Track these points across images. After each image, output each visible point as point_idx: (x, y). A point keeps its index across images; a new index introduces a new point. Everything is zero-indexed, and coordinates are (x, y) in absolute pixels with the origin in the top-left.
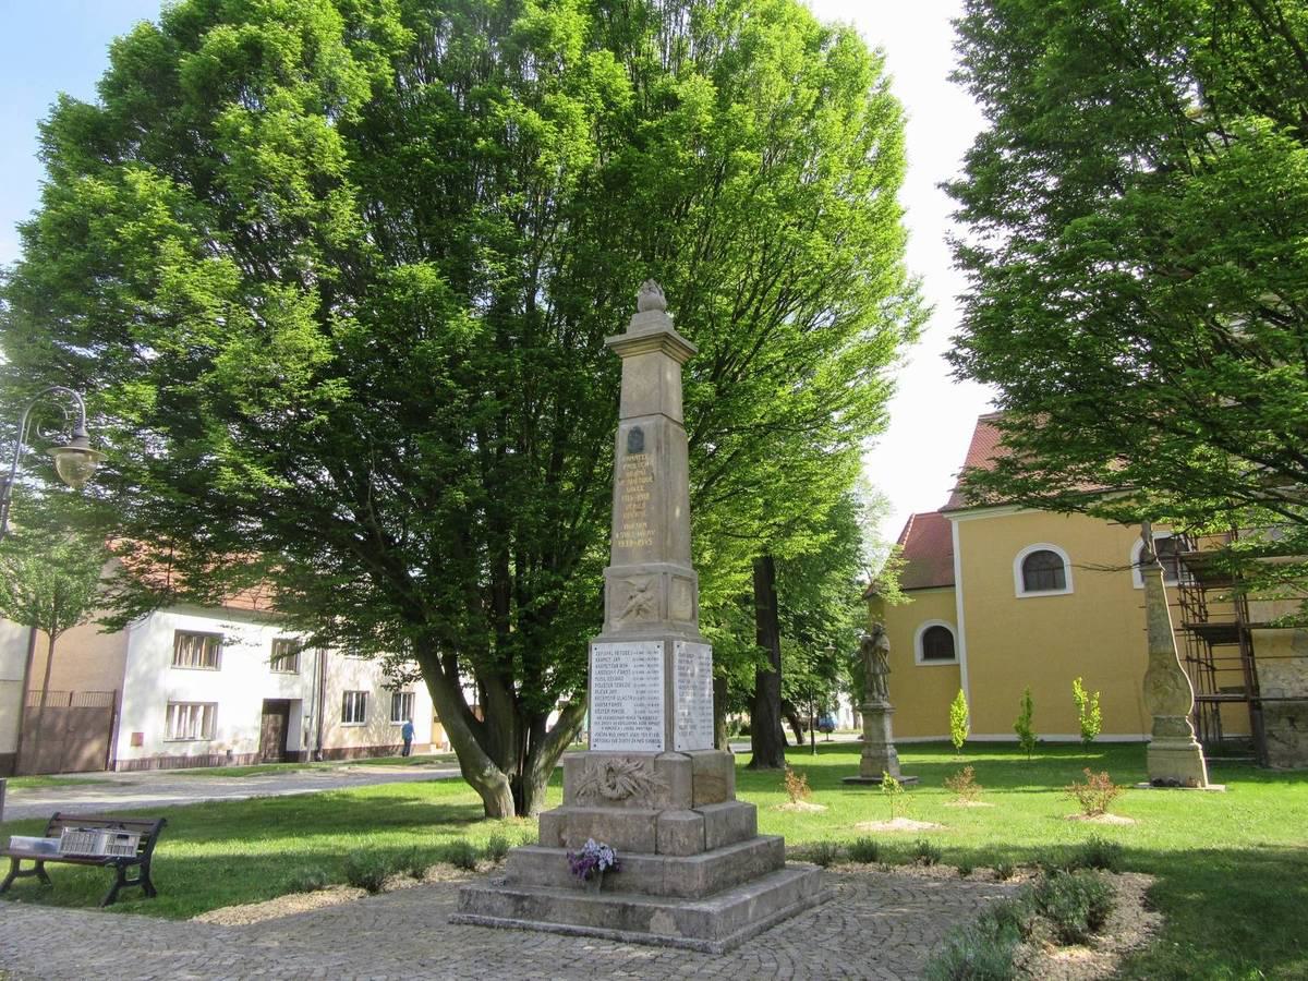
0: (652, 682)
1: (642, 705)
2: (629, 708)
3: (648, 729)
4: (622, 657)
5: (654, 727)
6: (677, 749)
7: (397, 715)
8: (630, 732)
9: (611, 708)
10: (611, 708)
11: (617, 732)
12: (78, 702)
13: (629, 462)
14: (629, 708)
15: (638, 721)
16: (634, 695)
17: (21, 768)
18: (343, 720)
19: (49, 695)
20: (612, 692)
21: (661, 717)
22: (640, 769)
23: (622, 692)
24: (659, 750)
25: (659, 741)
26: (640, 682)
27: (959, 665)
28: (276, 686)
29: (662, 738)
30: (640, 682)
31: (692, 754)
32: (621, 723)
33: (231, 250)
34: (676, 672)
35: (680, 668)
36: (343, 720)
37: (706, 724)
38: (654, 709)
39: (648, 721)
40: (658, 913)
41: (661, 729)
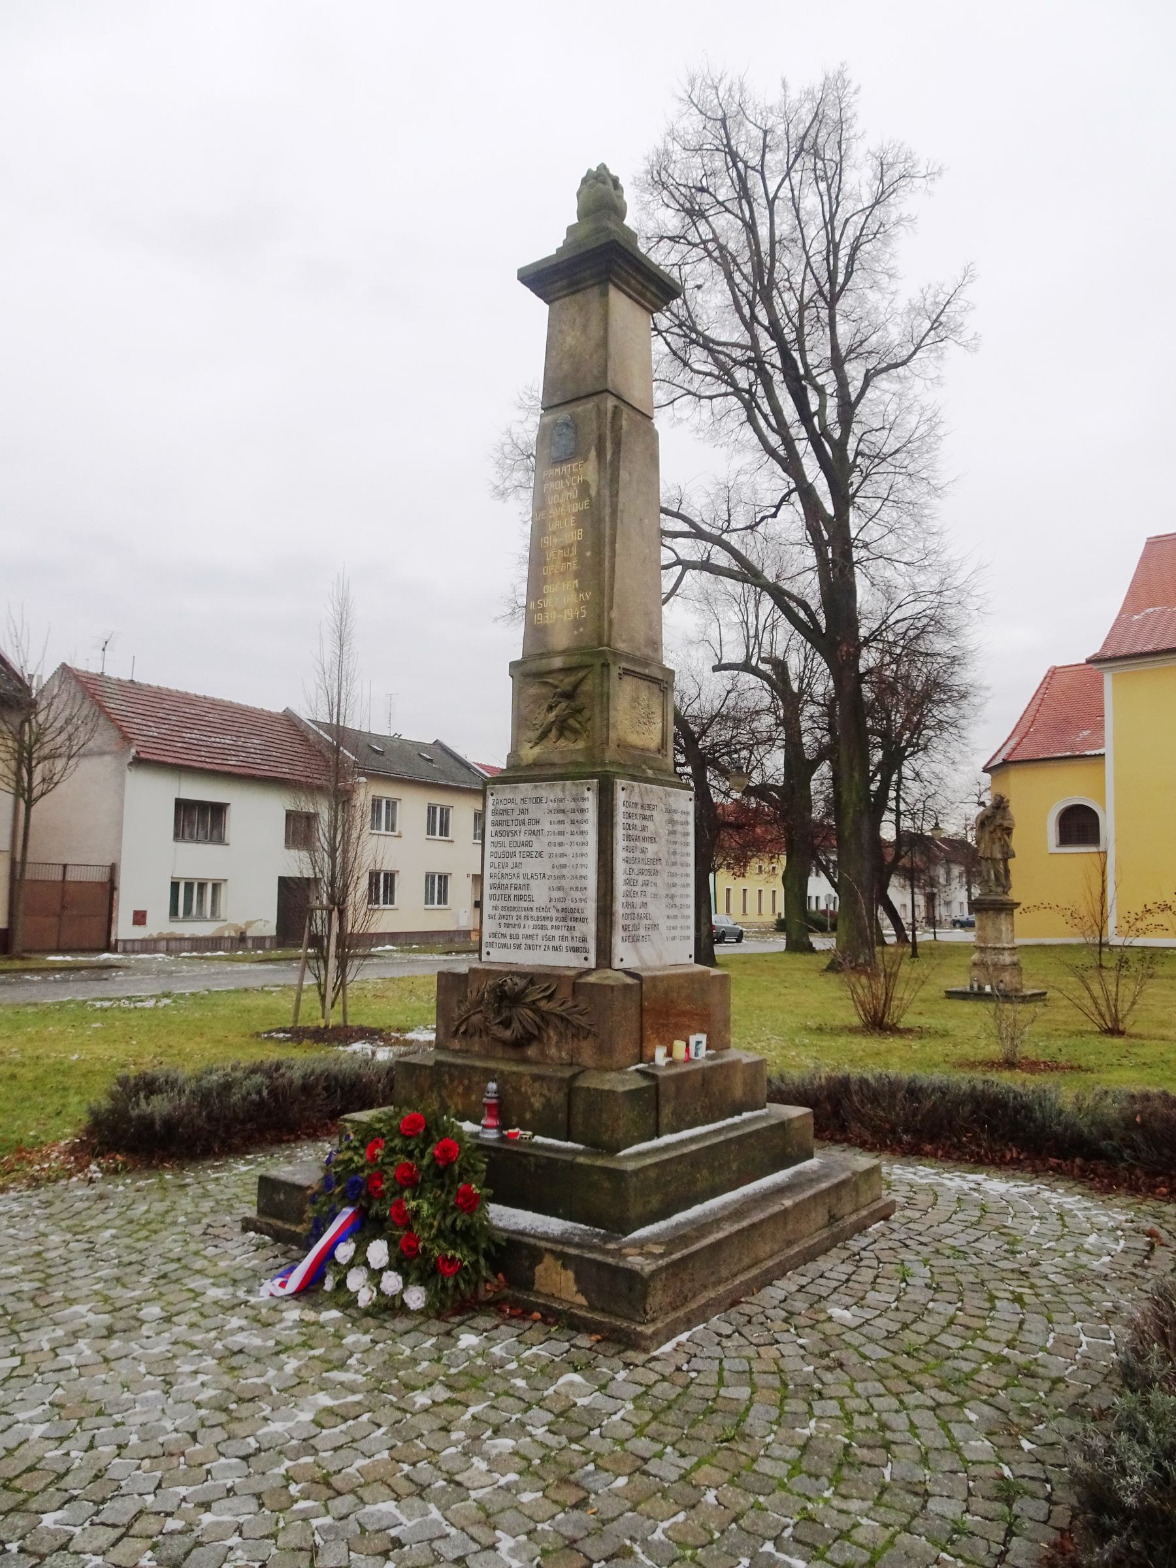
0: (577, 849)
1: (560, 888)
2: (541, 893)
3: (570, 929)
4: (531, 807)
5: (578, 925)
6: (616, 964)
7: (433, 898)
8: (540, 932)
9: (514, 892)
10: (514, 892)
11: (521, 932)
12: (73, 875)
13: (555, 479)
14: (541, 893)
15: (553, 913)
16: (548, 872)
17: (17, 948)
18: (426, 903)
19: (28, 867)
20: (516, 866)
21: (590, 909)
22: (550, 998)
23: (531, 866)
24: (586, 965)
25: (586, 950)
26: (557, 850)
27: (1105, 853)
28: (297, 864)
29: (592, 945)
30: (557, 850)
31: (644, 974)
32: (527, 918)
33: (898, 798)
34: (619, 833)
35: (627, 827)
36: (426, 903)
37: (679, 922)
38: (578, 895)
39: (569, 916)
40: (548, 1260)
41: (590, 929)
